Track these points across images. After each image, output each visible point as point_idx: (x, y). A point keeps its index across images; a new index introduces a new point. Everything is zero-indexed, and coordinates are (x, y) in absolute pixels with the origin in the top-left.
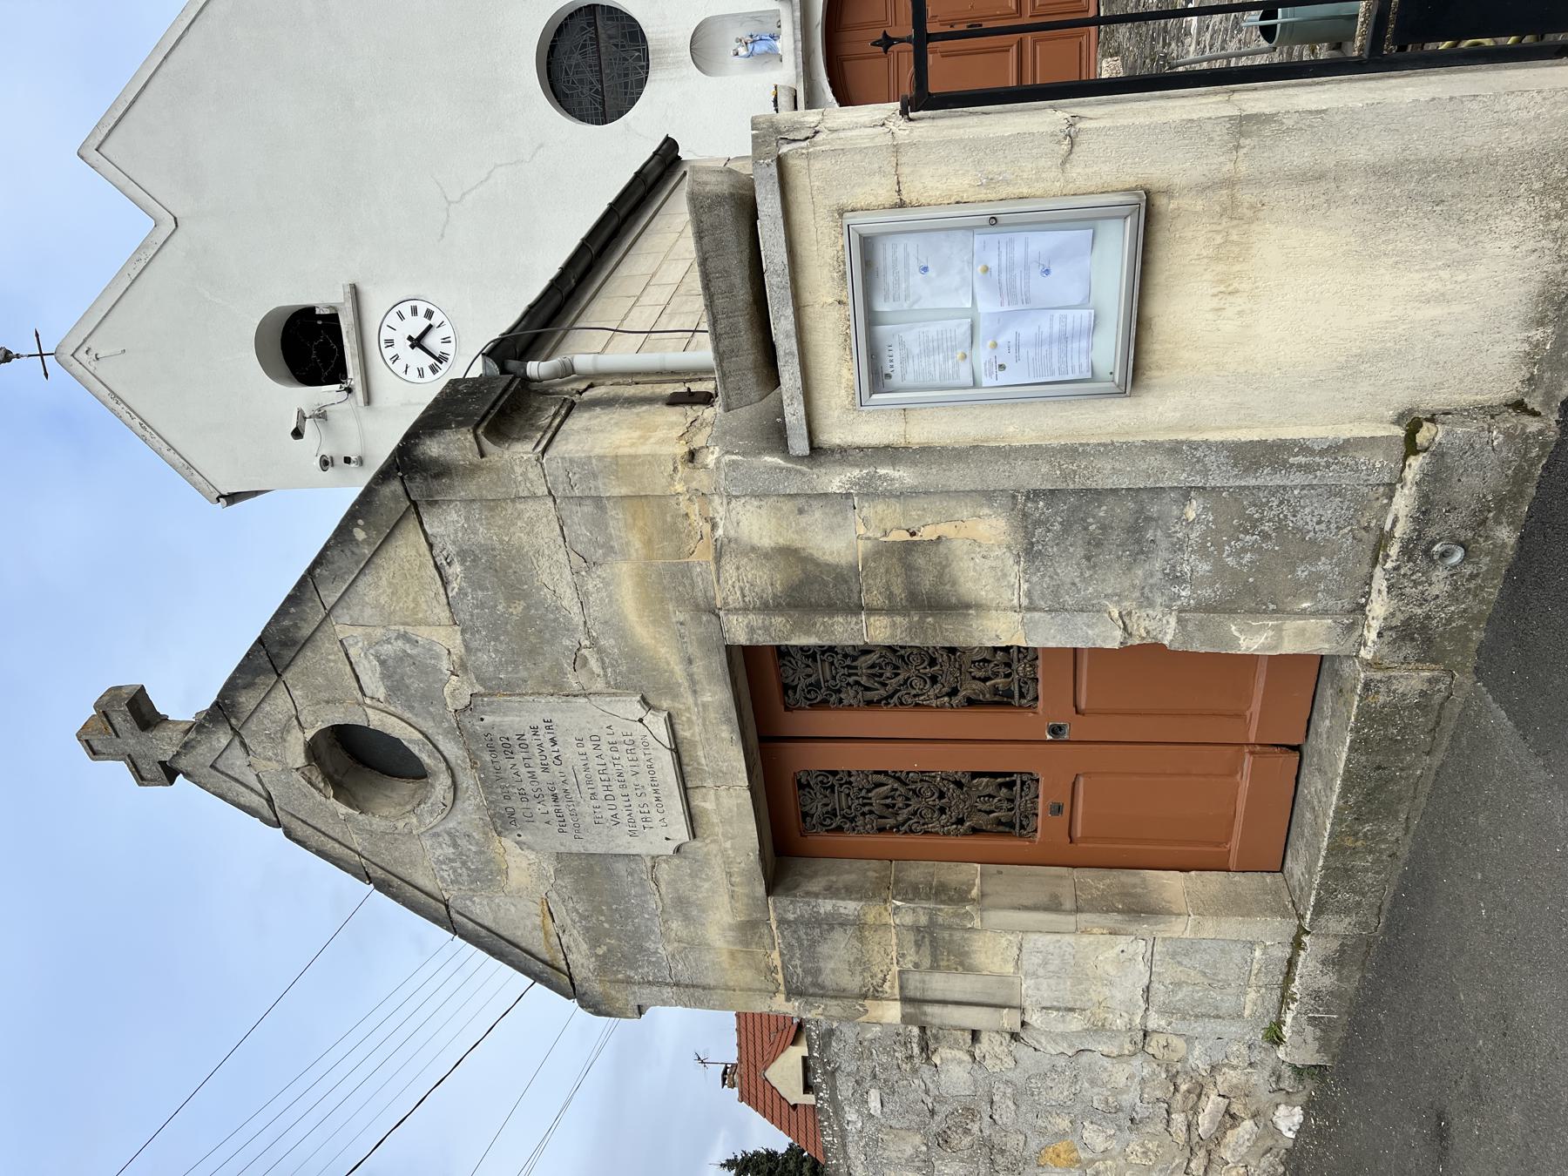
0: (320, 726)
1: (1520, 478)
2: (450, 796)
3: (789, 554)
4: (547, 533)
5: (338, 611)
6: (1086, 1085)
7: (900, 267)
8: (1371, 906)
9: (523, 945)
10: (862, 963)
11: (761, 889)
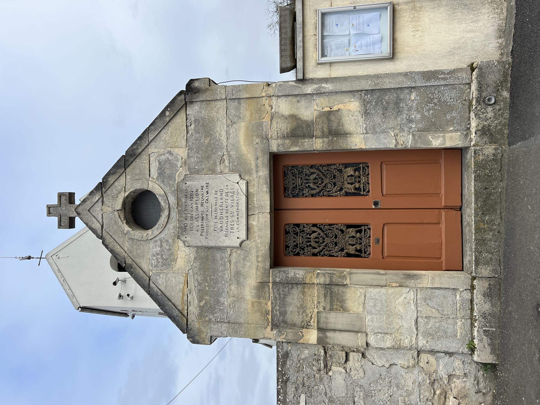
0: (132, 190)
1: (505, 75)
2: (166, 220)
3: (293, 117)
4: (222, 112)
5: (152, 143)
7: (331, 24)
8: (496, 259)
9: (173, 301)
10: (303, 308)
11: (268, 264)
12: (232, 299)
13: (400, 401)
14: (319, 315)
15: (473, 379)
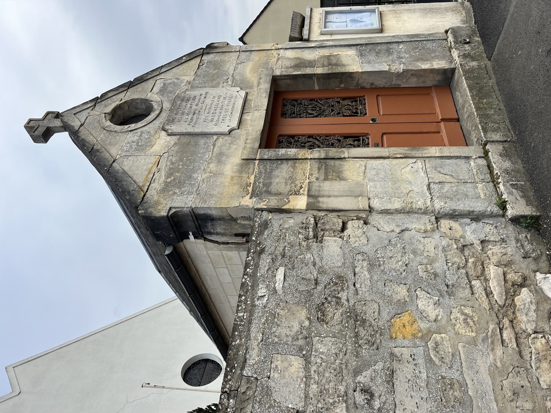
2: (155, 117)
6: (412, 256)
10: (292, 179)
11: (257, 145)
12: (208, 174)
13: (420, 270)
14: (311, 184)
15: (514, 242)
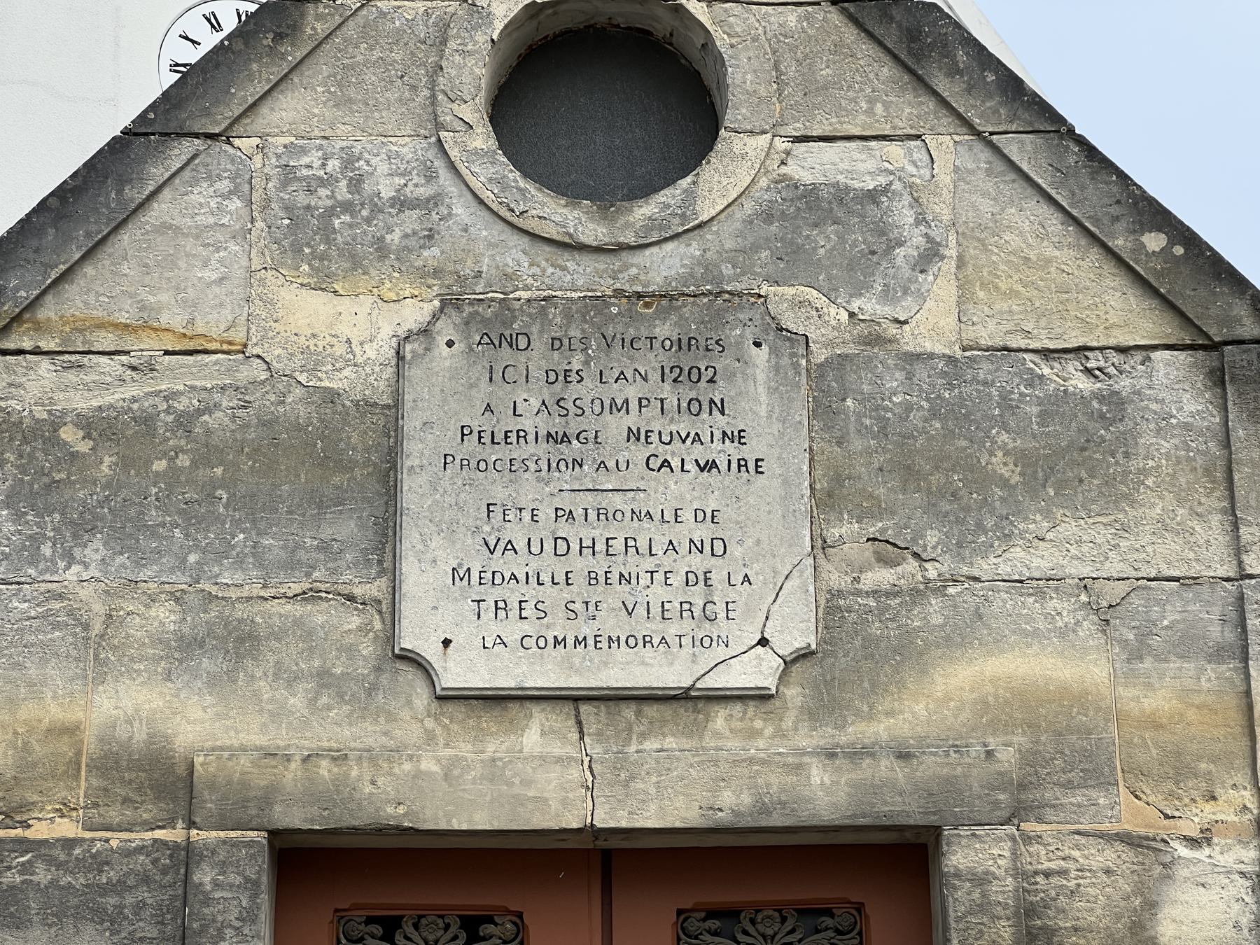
2: (552, 232)
4: (1166, 555)
5: (985, 154)
11: (293, 817)
